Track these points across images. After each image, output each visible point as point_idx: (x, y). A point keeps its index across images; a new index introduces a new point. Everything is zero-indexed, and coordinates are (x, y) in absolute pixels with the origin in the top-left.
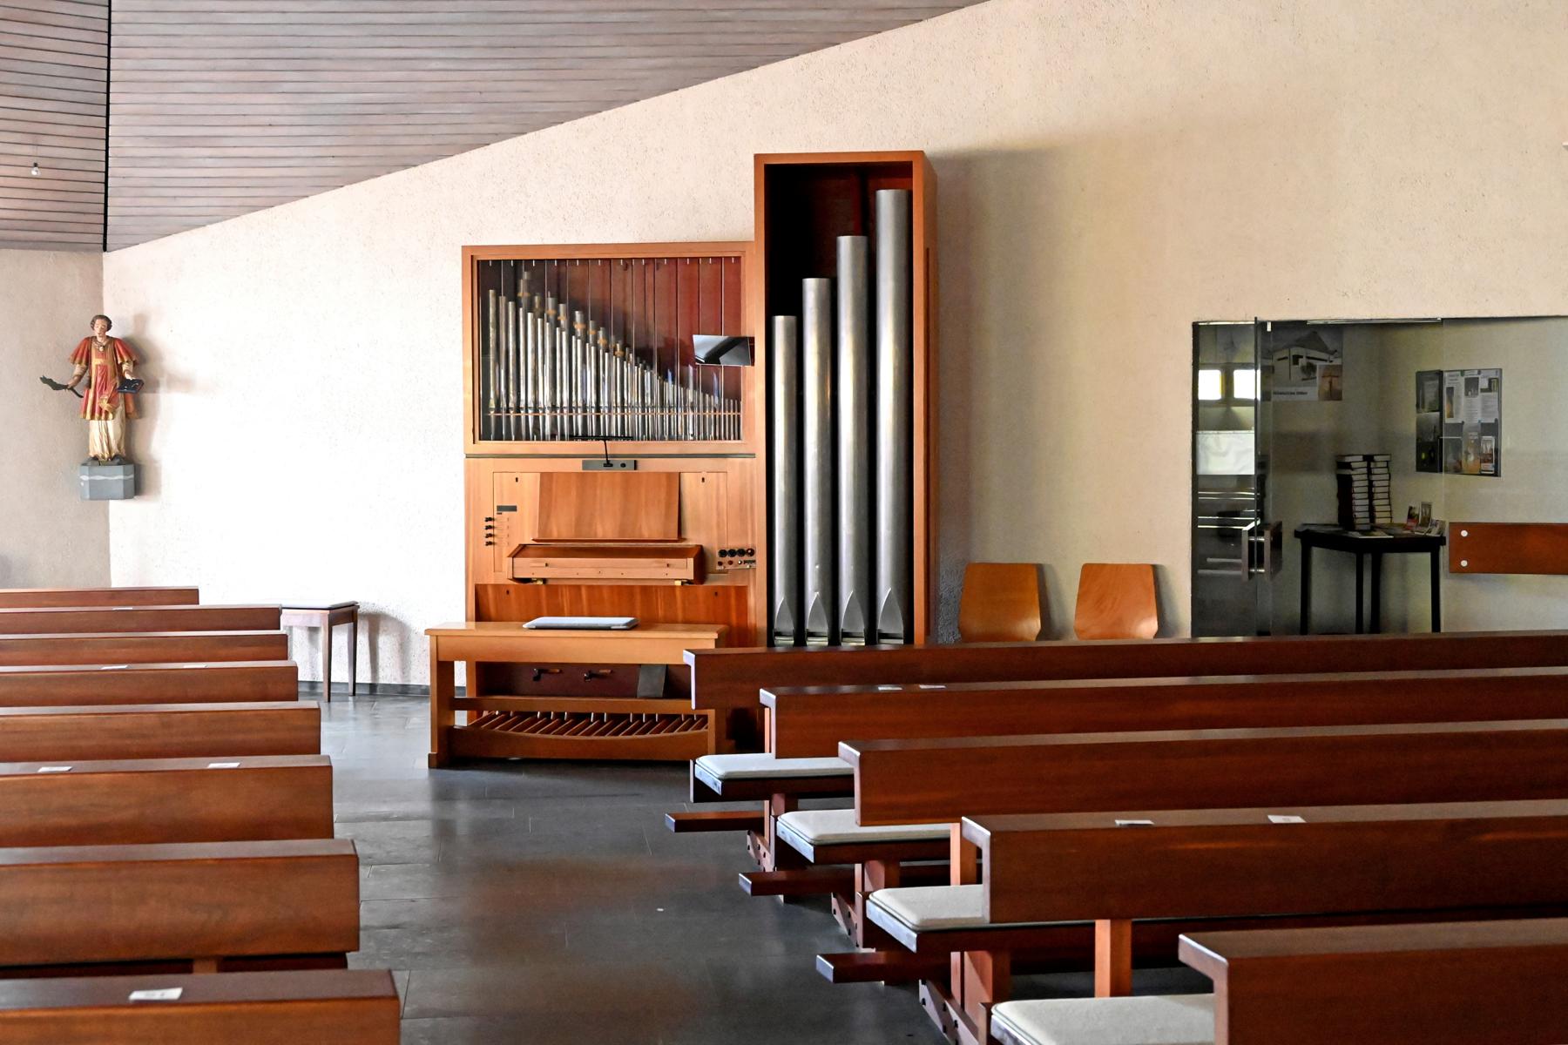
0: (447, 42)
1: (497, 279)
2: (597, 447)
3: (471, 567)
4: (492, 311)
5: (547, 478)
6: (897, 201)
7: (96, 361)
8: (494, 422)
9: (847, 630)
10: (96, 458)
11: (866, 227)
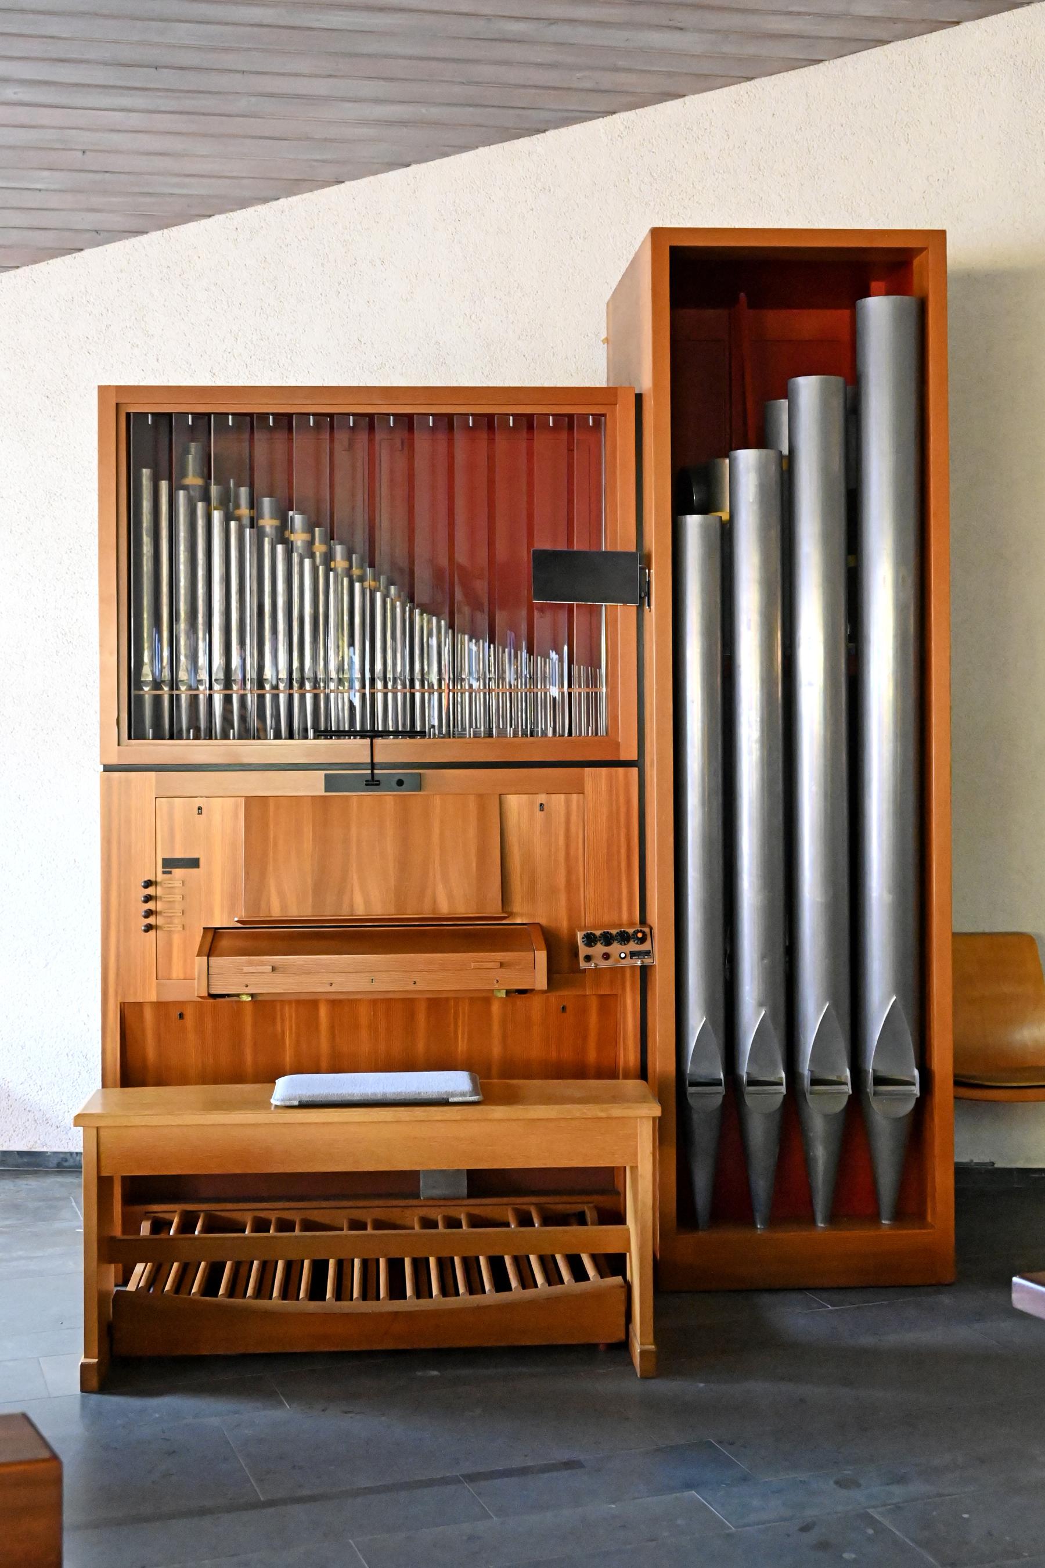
0: (37, 48)
1: (167, 447)
2: (356, 750)
3: (114, 969)
4: (146, 505)
5: (257, 809)
6: (898, 318)
8: (149, 713)
9: (885, 1072)
11: (844, 365)
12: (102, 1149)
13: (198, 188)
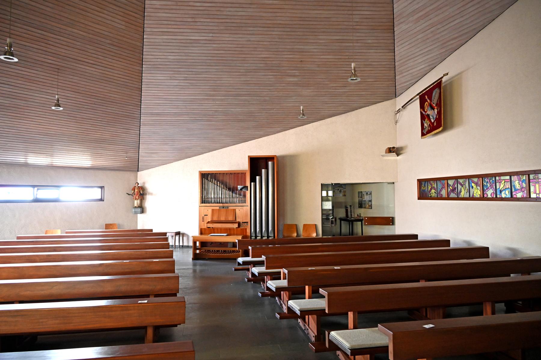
1: (205, 176)
2: (221, 205)
5: (213, 210)
8: (204, 201)
12: (363, 185)
13: (361, 105)
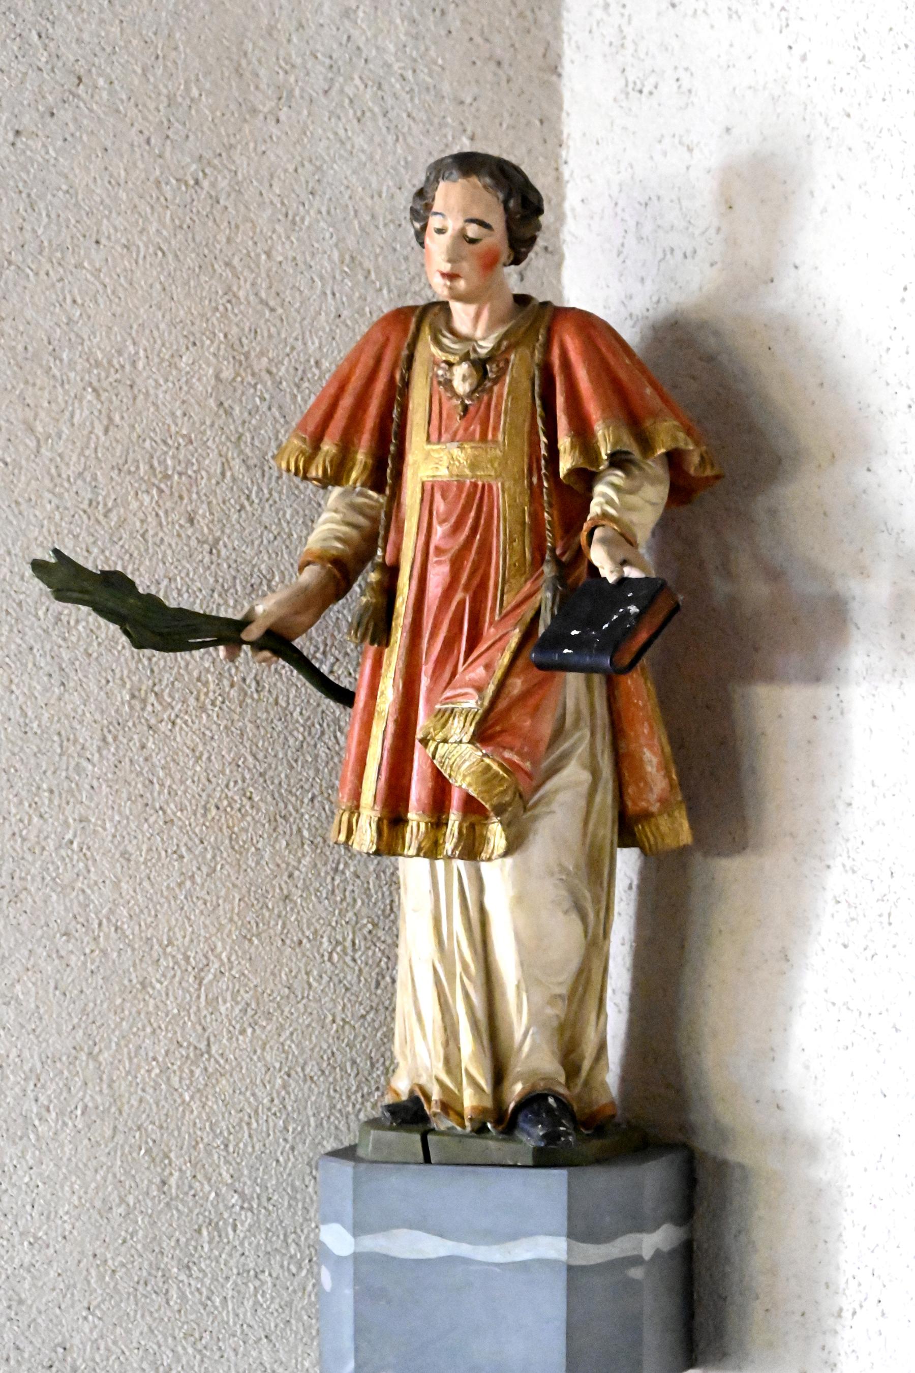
7: (431, 461)
10: (410, 1114)
